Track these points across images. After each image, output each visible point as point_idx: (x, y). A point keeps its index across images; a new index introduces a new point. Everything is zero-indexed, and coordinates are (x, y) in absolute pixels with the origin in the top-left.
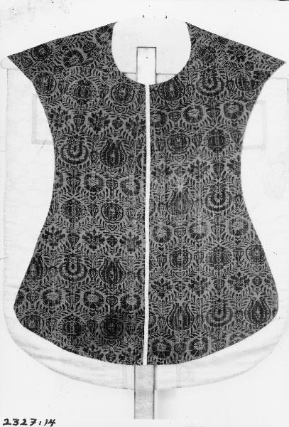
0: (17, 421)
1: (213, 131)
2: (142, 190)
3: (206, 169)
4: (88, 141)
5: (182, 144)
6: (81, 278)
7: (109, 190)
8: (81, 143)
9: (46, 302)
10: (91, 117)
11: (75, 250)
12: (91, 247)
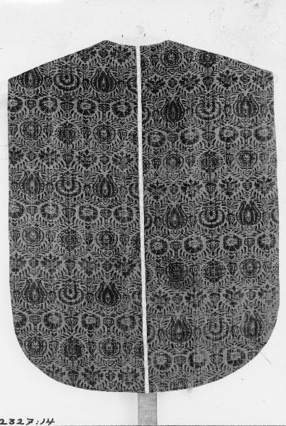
0: (12, 421)
1: (207, 153)
2: (135, 217)
3: (202, 298)
4: (79, 176)
5: (175, 60)
6: (76, 194)
7: (101, 112)
8: (75, 286)
9: (44, 215)
10: (78, 154)
11: (72, 276)
12: (83, 59)
